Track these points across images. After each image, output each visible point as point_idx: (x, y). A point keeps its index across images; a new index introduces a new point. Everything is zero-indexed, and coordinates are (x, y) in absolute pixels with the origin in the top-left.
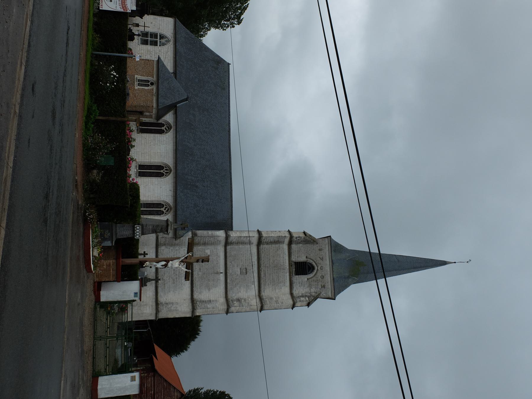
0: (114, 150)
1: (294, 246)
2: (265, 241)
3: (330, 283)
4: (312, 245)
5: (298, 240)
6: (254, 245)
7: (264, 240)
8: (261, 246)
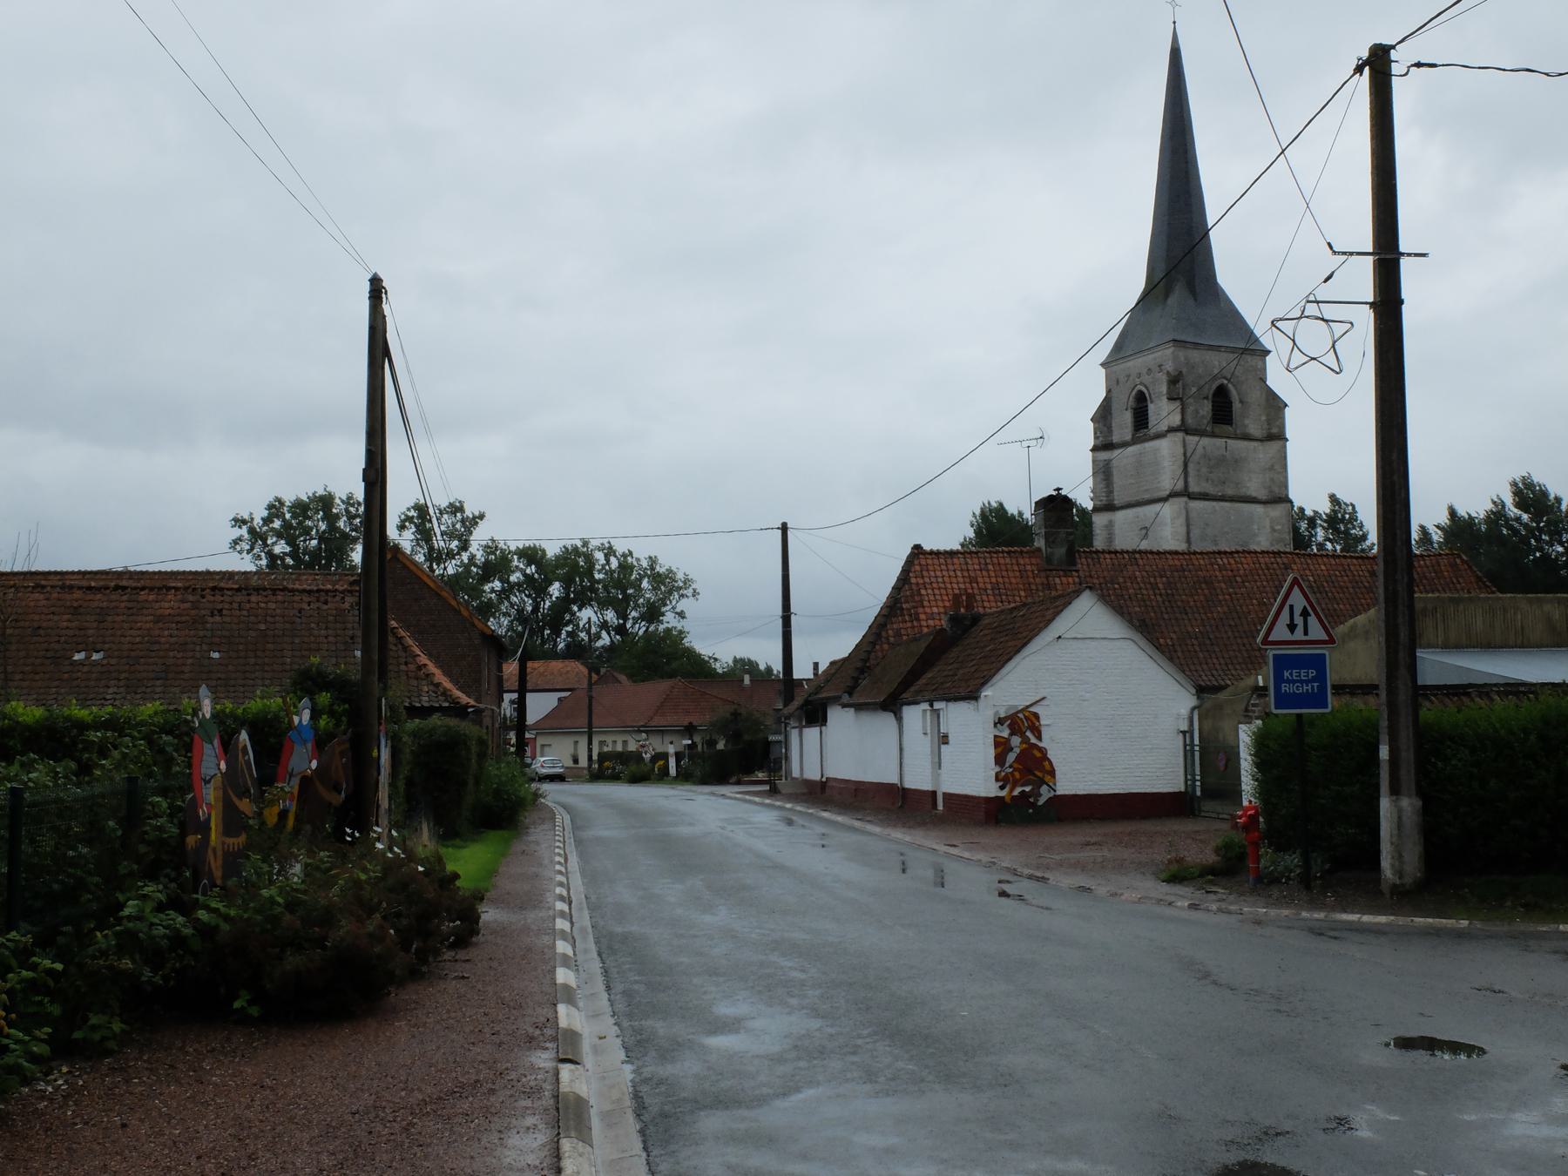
0: (1030, 814)
1: (1116, 439)
2: (1105, 499)
3: (1156, 355)
4: (1113, 399)
5: (1101, 433)
6: (1113, 518)
7: (1101, 501)
8: (1116, 502)
